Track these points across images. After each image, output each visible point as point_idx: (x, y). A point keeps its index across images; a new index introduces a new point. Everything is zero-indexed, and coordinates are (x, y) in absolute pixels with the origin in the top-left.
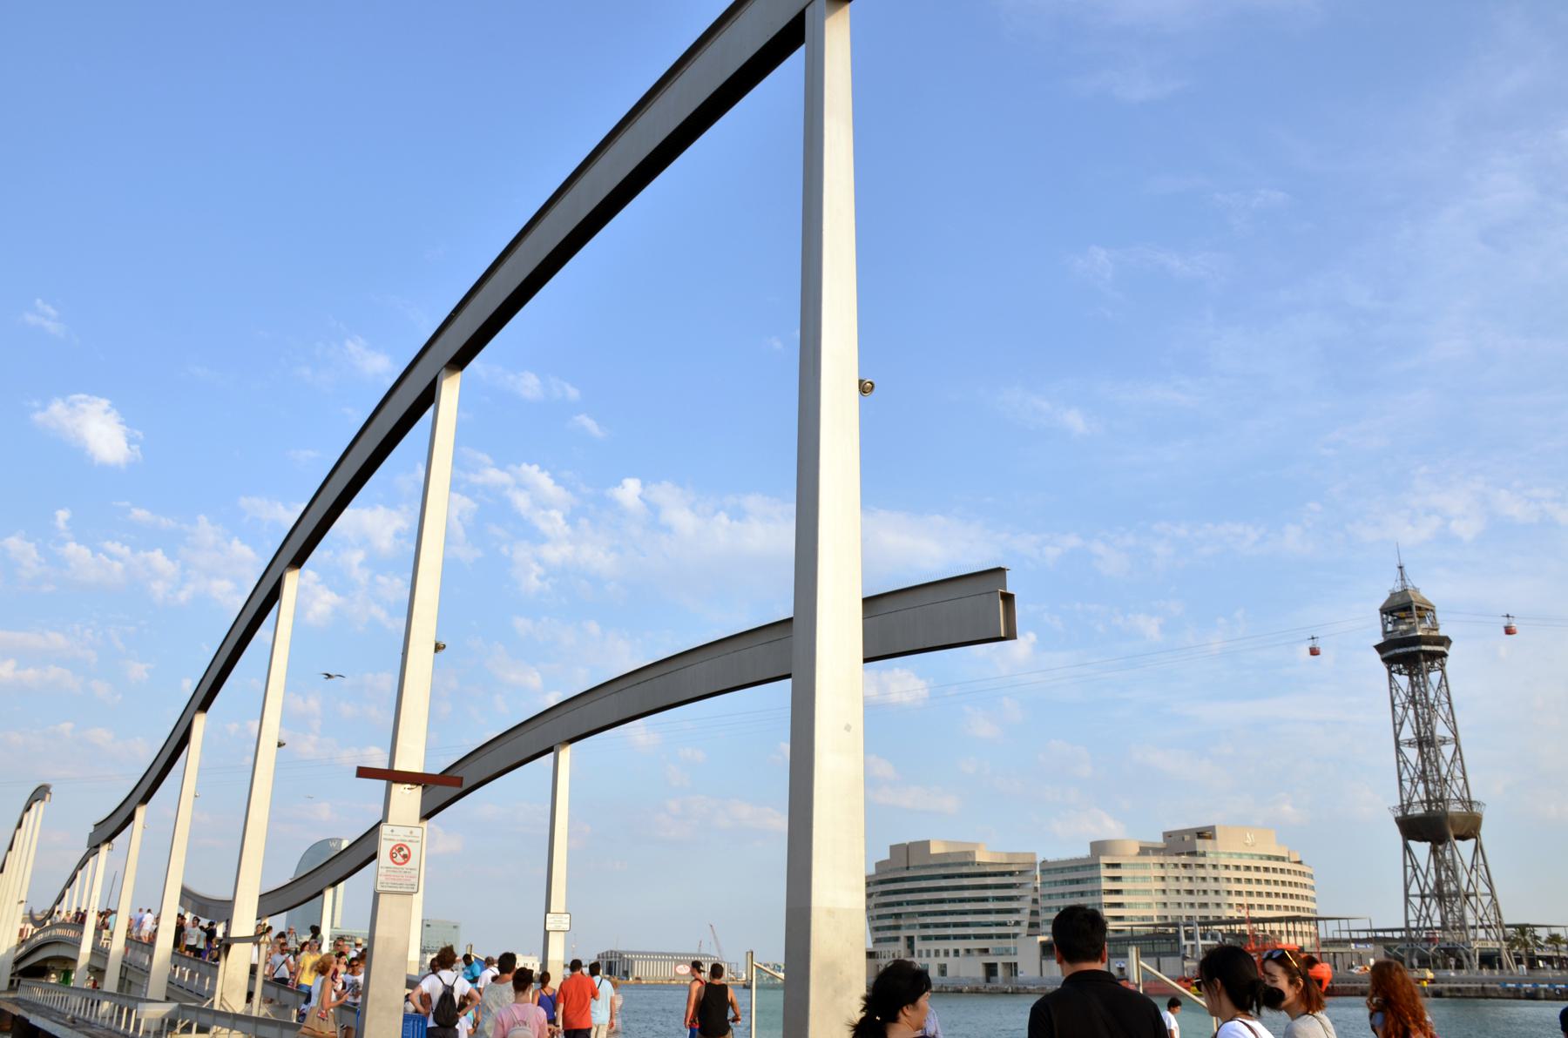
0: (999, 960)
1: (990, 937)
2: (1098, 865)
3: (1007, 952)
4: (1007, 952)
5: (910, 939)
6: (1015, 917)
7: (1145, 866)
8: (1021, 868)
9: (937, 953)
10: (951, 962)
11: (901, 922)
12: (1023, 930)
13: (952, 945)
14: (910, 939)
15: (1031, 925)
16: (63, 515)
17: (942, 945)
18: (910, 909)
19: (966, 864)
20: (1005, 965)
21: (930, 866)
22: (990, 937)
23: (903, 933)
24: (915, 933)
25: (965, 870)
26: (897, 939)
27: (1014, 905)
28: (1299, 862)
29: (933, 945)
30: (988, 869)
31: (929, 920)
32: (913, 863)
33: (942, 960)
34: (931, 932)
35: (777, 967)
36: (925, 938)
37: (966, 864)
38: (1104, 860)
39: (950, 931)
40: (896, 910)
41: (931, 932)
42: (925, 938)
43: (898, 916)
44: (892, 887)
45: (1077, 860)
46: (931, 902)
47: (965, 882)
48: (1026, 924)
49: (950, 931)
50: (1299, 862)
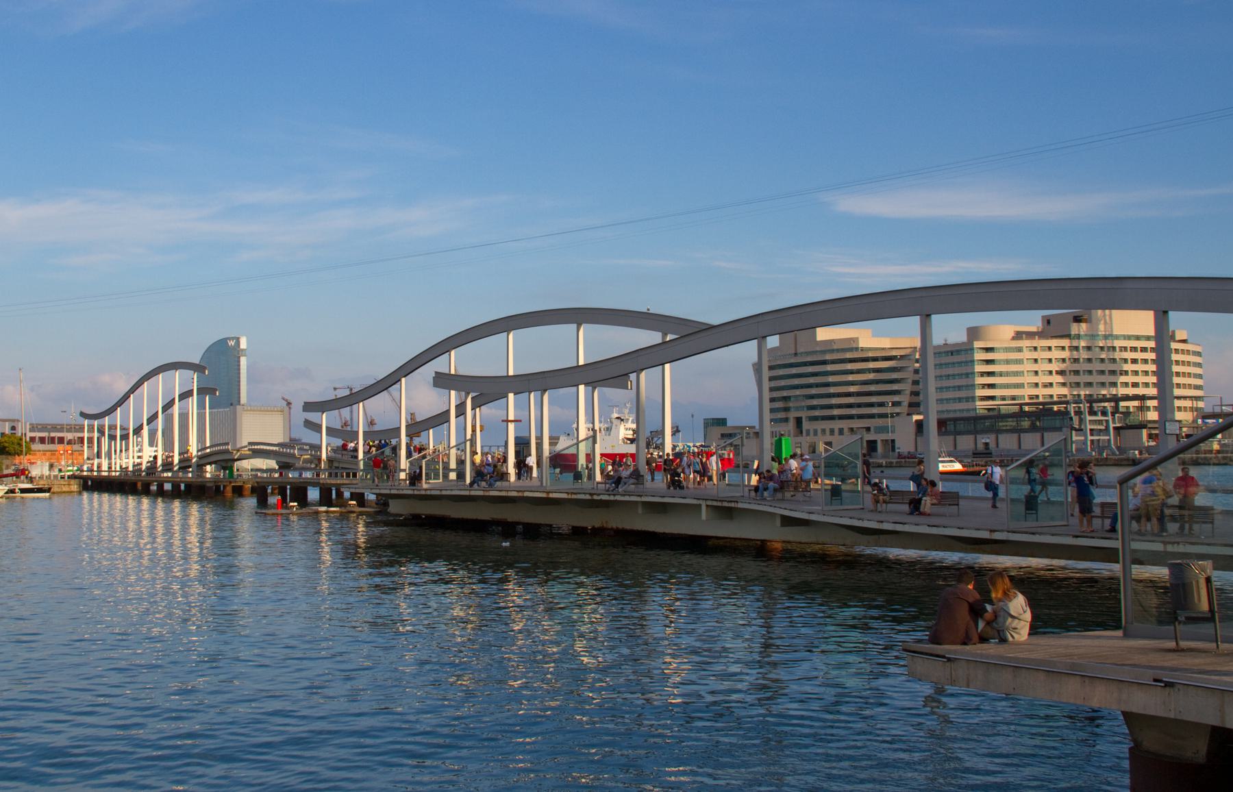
0: (879, 438)
1: (872, 416)
2: (972, 349)
3: (883, 429)
4: (883, 429)
5: (799, 421)
6: (896, 398)
7: (1020, 350)
8: (902, 353)
9: (841, 431)
10: (835, 439)
11: (791, 405)
12: (903, 409)
13: (837, 425)
14: (799, 421)
15: (911, 405)
16: (208, 475)
17: (828, 425)
18: (798, 392)
19: (851, 350)
20: (885, 442)
21: (815, 352)
22: (872, 416)
23: (792, 415)
24: (803, 414)
25: (849, 355)
26: (786, 420)
27: (895, 387)
28: (1184, 341)
29: (820, 425)
30: (870, 355)
31: (815, 402)
32: (800, 350)
33: (829, 438)
34: (817, 413)
35: (1148, 338)
36: (815, 418)
37: (851, 350)
38: (977, 344)
39: (836, 412)
40: (785, 393)
41: (817, 413)
42: (815, 418)
43: (786, 399)
44: (794, 371)
45: (957, 344)
46: (817, 385)
47: (850, 366)
48: (906, 404)
49: (854, 411)
50: (1184, 341)
